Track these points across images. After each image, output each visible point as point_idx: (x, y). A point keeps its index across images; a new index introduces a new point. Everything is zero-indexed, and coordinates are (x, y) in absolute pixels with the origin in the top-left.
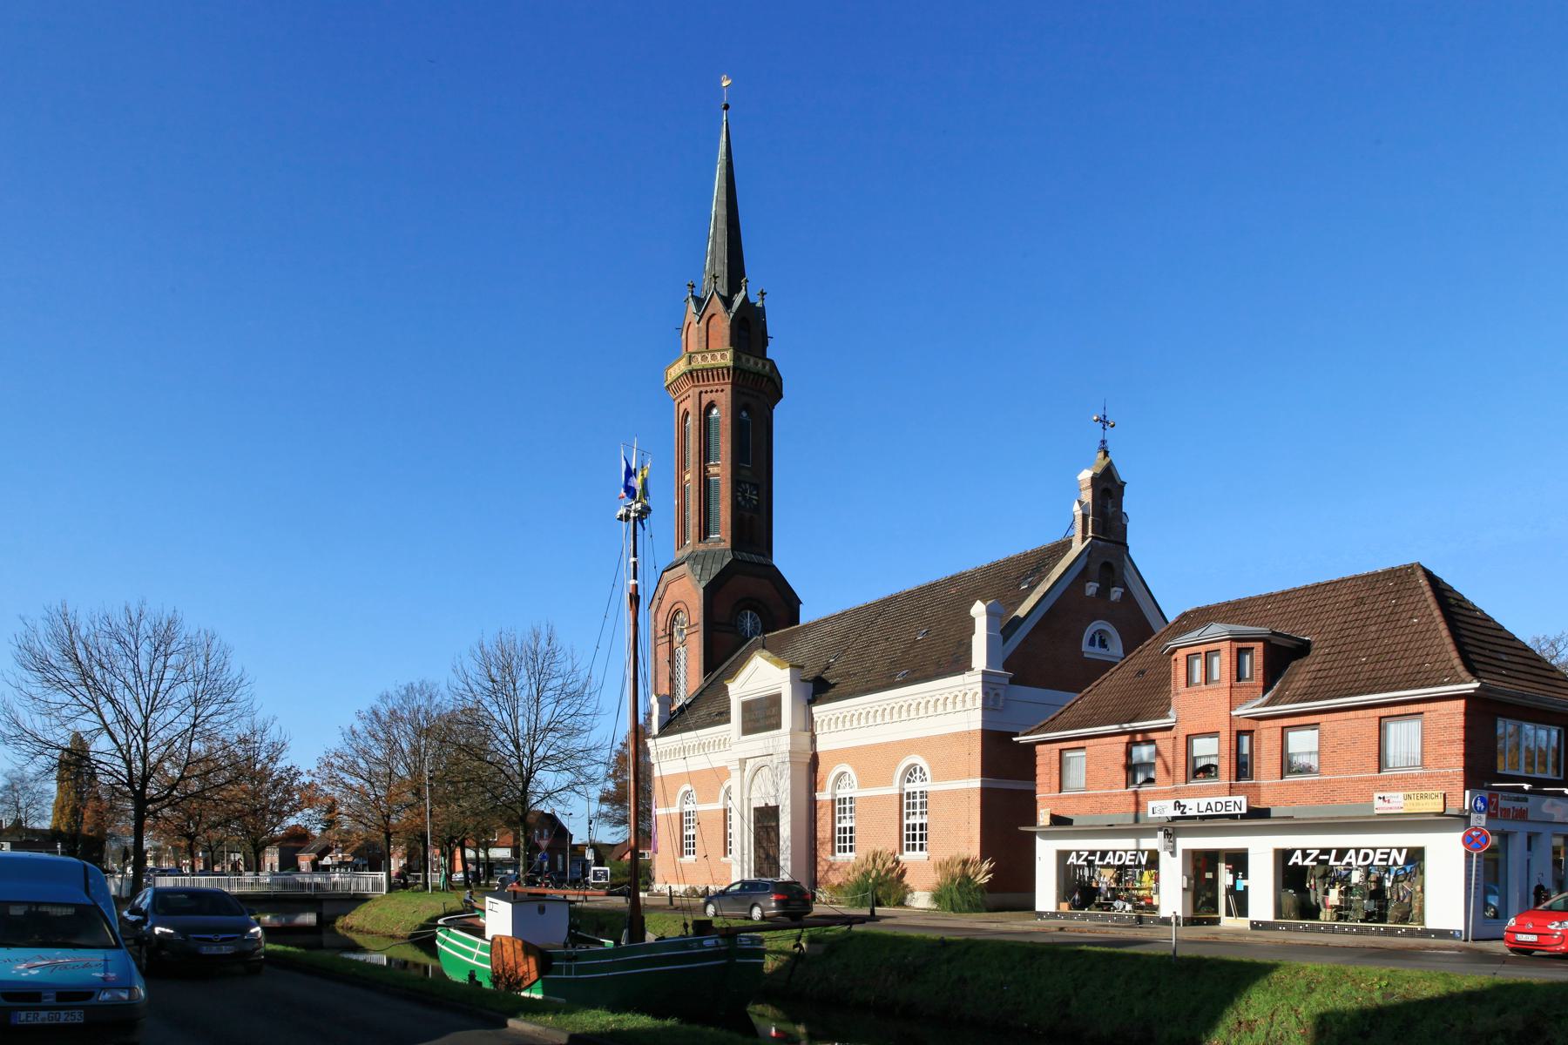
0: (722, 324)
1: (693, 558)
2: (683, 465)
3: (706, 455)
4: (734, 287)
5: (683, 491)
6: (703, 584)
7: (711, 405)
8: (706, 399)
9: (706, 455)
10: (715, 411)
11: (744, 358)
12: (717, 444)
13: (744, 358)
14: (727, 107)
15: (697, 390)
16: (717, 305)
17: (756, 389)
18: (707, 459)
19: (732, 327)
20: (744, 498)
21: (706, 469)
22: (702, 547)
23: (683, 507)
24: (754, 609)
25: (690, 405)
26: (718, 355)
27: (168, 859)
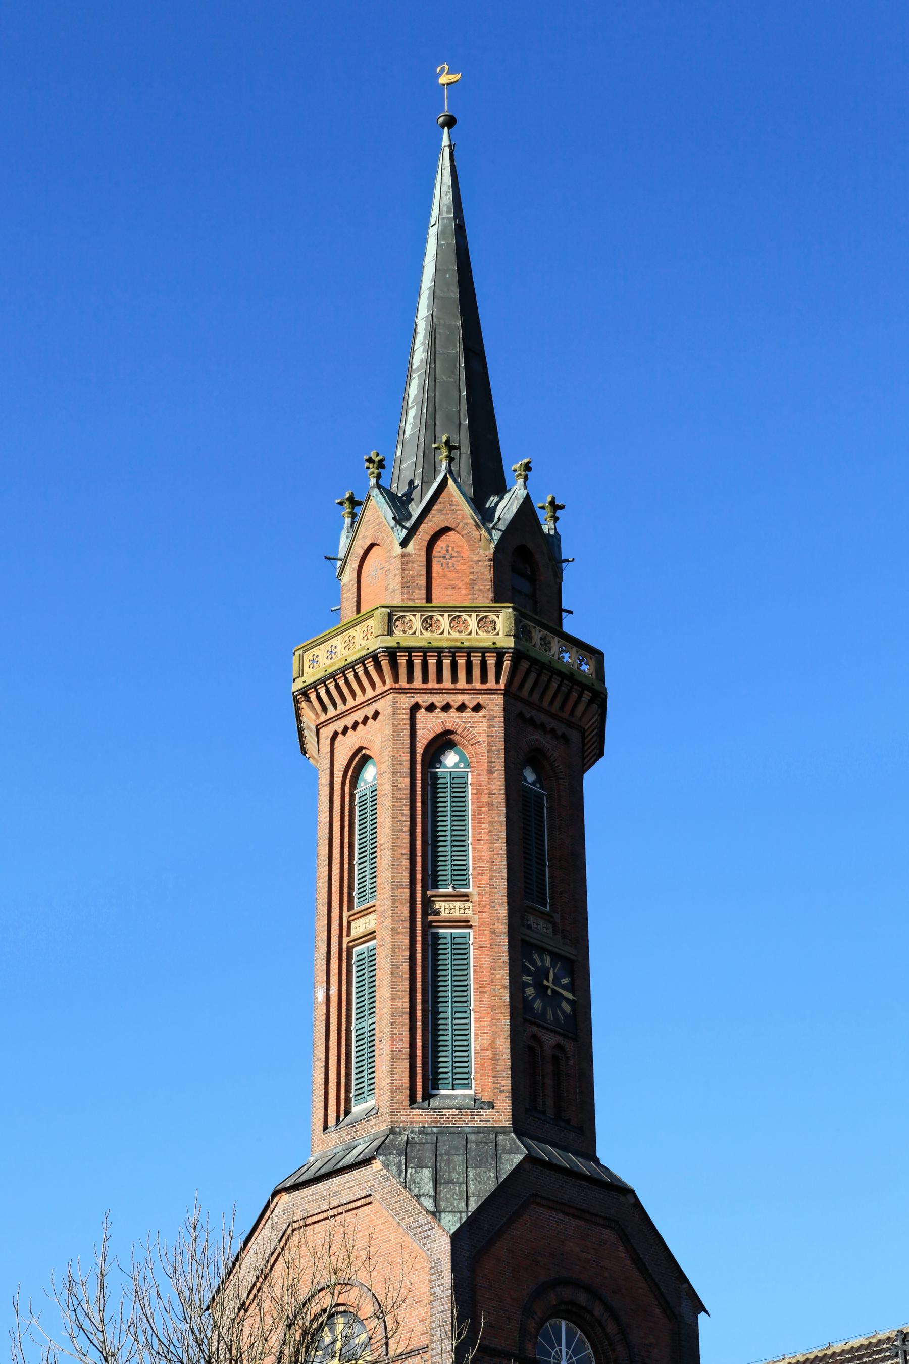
0: (470, 556)
1: (399, 1149)
2: (347, 893)
3: (429, 863)
4: (487, 480)
5: (347, 967)
6: (452, 1222)
7: (444, 742)
8: (429, 726)
9: (429, 863)
10: (369, 773)
11: (537, 635)
12: (460, 841)
13: (537, 635)
14: (450, 122)
15: (406, 701)
16: (457, 504)
17: (556, 717)
18: (432, 879)
19: (497, 560)
20: (541, 989)
21: (427, 903)
22: (419, 1119)
23: (345, 1008)
24: (575, 1314)
25: (382, 737)
26: (472, 621)
27: (456, 765)
